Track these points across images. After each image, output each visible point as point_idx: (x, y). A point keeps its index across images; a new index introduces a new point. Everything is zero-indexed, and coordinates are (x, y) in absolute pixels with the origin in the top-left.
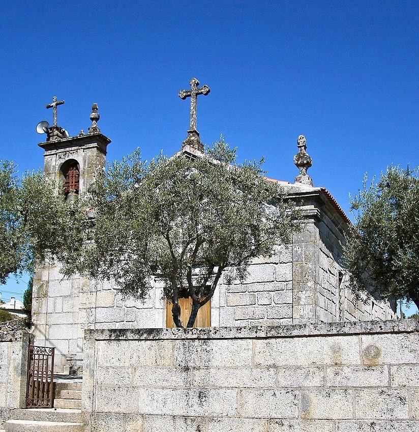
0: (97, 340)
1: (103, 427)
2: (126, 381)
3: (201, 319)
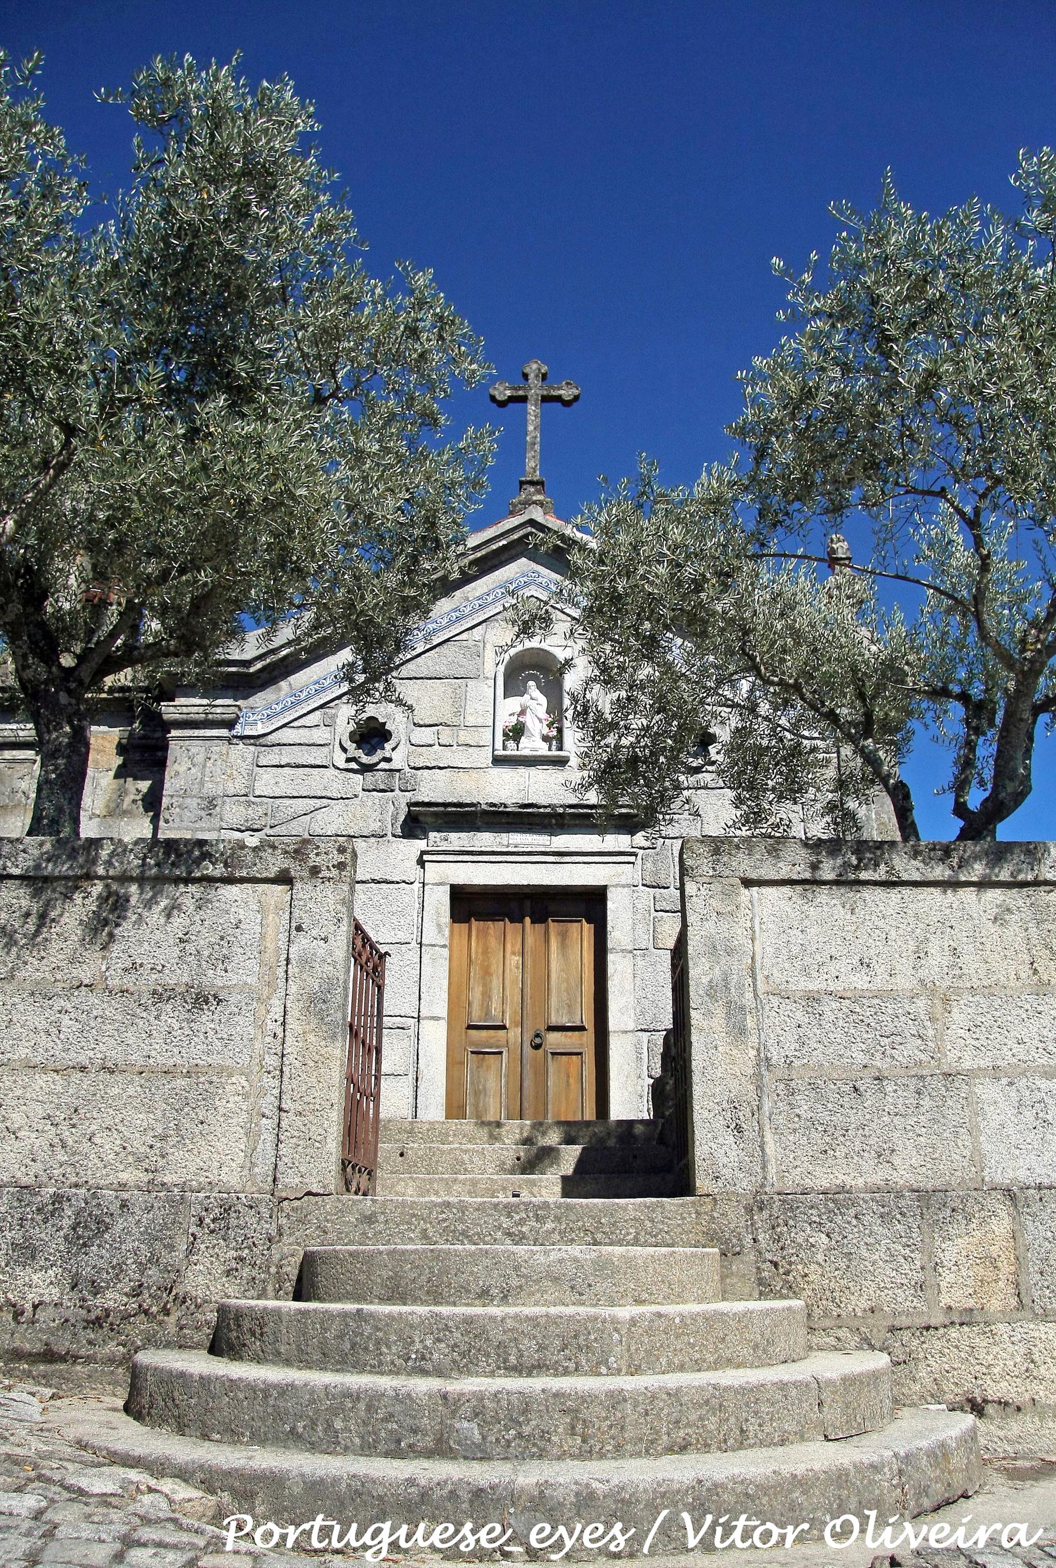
0: (748, 883)
1: (820, 1258)
2: (909, 1051)
3: (564, 986)
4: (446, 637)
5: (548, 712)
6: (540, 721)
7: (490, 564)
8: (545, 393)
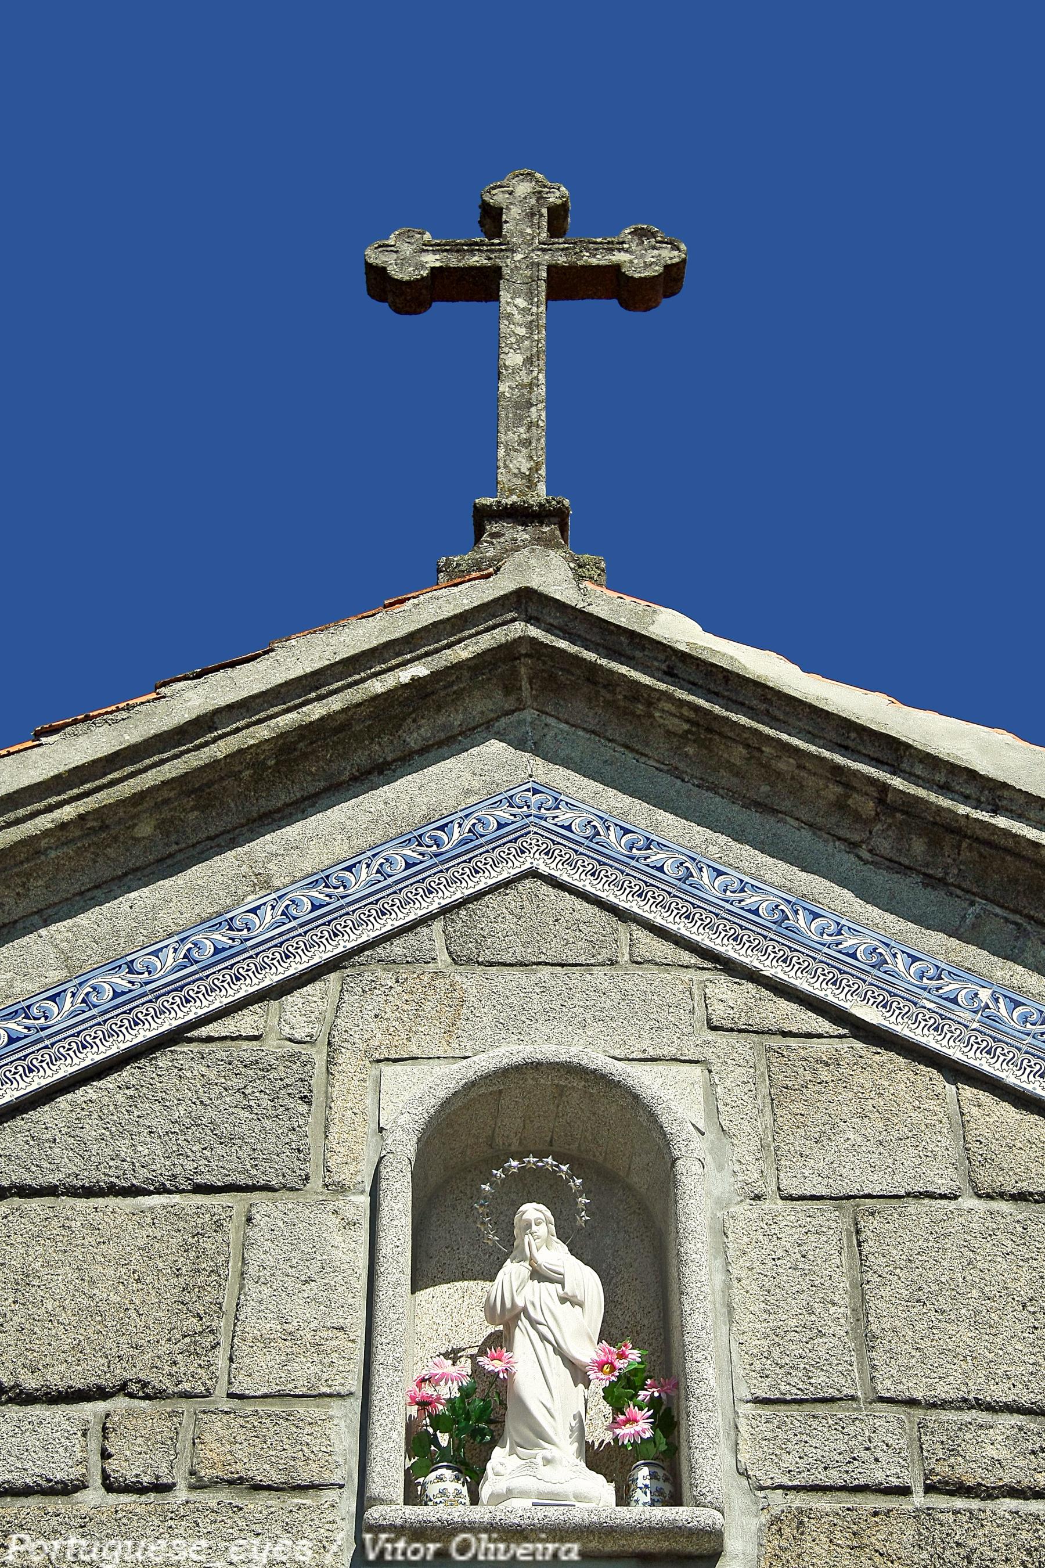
4: (168, 1023)
5: (608, 1334)
6: (579, 1374)
7: (360, 758)
8: (562, 260)
